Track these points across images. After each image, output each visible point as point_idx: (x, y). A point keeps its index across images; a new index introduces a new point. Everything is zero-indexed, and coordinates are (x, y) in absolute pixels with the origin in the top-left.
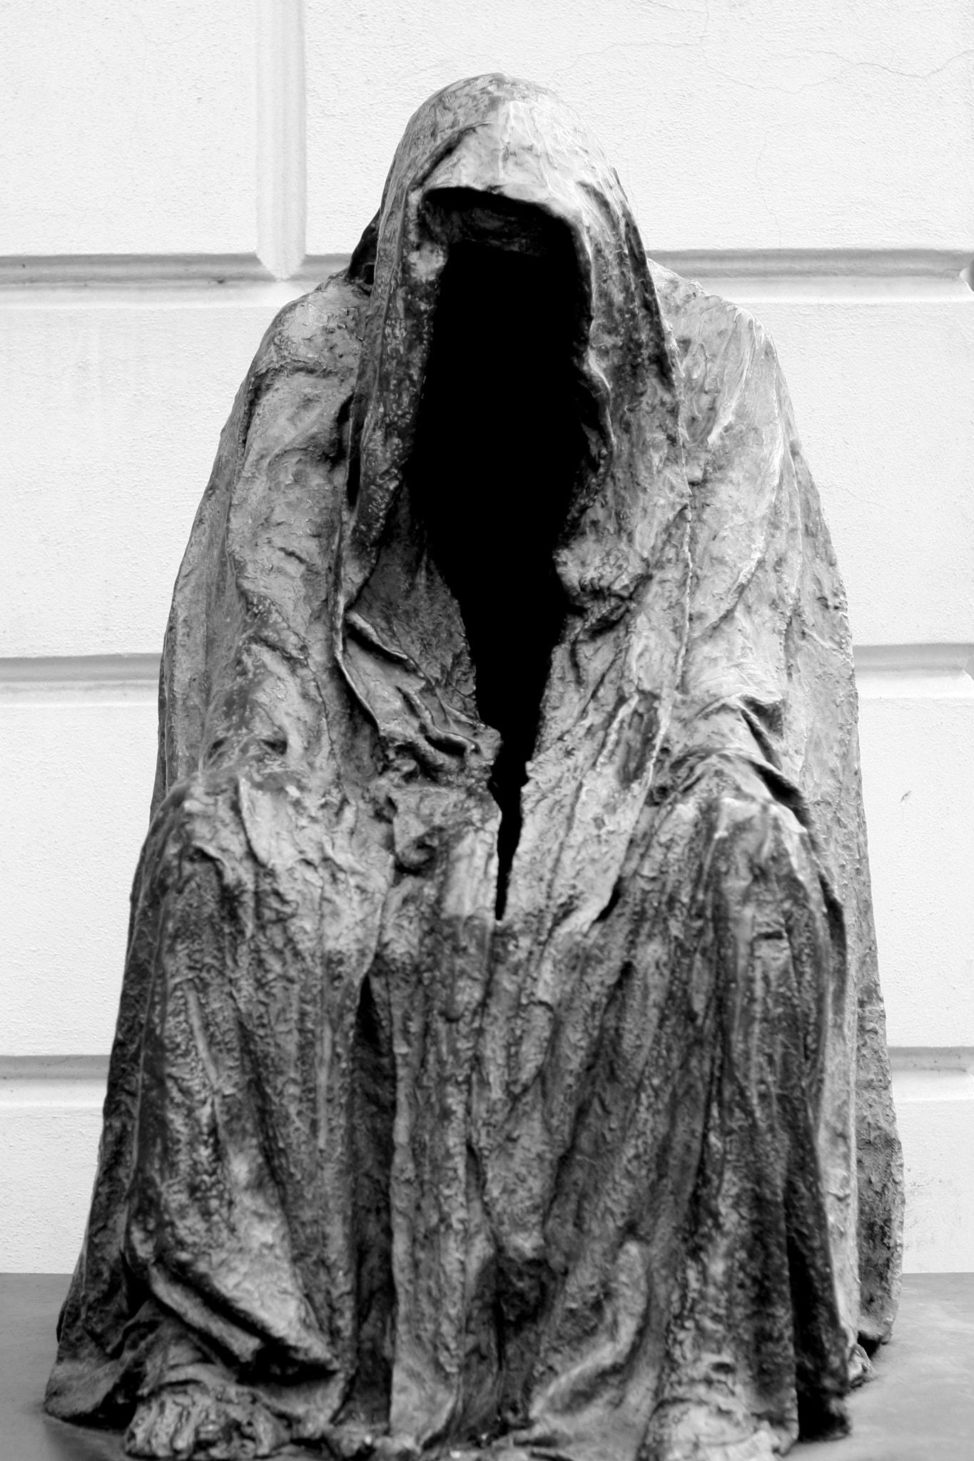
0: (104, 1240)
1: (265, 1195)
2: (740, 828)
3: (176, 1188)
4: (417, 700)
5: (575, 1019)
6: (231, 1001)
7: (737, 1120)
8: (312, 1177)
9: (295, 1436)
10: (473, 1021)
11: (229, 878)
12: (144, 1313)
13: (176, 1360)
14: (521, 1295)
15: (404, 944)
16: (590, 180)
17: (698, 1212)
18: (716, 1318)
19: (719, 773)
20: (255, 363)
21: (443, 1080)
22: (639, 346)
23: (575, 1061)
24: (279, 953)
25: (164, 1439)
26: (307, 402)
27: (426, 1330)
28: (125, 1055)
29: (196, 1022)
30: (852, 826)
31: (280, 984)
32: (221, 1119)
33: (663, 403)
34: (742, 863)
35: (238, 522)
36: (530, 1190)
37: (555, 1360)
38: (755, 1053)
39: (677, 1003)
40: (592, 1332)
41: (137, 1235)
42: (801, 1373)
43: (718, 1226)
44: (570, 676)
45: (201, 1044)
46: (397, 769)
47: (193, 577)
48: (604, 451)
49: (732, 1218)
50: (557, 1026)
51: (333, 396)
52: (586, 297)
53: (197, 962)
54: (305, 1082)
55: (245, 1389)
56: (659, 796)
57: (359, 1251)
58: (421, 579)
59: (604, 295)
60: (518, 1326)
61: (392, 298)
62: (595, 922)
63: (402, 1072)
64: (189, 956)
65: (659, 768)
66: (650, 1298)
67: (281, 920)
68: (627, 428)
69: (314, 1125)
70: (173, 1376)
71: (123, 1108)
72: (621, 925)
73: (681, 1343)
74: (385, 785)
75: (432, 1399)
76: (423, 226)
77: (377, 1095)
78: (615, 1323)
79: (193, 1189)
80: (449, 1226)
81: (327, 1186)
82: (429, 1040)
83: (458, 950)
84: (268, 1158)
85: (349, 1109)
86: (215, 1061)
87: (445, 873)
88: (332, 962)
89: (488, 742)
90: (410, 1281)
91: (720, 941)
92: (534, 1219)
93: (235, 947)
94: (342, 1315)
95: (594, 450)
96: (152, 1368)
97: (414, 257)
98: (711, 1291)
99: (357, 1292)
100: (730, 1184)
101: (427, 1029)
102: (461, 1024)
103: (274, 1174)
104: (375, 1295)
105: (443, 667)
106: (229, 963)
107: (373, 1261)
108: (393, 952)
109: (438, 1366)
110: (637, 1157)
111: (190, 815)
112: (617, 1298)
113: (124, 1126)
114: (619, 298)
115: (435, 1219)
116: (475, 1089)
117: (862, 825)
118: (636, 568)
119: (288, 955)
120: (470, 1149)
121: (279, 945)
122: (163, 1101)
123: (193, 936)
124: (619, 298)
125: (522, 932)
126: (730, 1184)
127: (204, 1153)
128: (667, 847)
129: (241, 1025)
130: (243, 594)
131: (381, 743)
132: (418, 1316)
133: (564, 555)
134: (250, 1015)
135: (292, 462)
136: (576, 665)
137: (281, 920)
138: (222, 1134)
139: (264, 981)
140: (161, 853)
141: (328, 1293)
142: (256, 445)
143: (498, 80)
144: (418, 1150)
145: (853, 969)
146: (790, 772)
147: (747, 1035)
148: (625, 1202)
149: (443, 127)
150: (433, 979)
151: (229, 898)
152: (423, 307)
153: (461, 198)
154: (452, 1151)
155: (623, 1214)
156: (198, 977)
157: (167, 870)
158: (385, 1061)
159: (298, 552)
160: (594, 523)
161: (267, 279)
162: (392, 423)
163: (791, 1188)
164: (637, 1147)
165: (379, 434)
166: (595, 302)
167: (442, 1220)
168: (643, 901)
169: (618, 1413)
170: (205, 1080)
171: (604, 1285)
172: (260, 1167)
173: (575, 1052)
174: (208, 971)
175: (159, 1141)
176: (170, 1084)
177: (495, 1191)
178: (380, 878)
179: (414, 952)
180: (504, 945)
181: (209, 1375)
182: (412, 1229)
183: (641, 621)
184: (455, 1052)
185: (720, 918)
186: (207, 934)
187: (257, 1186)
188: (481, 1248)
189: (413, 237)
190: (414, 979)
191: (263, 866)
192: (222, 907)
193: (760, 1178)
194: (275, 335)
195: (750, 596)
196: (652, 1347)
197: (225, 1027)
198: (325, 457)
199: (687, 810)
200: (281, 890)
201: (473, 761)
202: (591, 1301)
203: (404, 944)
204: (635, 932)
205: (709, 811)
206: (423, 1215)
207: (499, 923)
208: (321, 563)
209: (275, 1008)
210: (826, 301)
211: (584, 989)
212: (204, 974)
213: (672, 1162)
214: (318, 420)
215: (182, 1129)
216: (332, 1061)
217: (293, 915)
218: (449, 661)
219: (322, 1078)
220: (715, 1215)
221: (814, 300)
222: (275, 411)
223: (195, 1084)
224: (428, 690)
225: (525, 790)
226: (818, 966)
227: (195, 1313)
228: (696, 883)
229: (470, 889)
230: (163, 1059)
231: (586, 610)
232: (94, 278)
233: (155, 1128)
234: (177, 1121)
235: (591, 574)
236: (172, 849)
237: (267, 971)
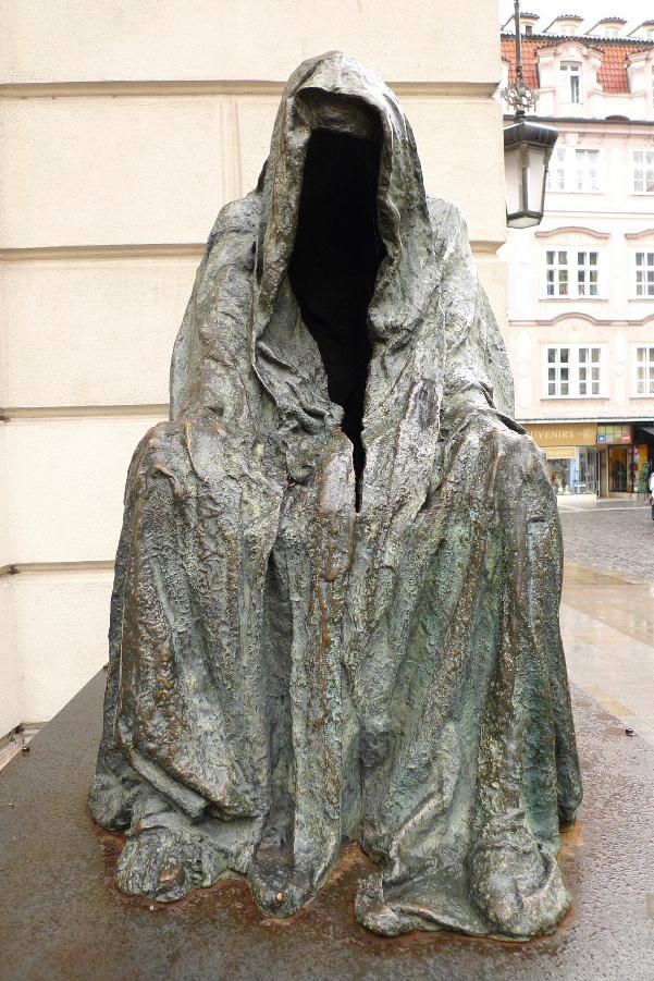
4: (297, 388)
10: (343, 580)
11: (179, 488)
15: (296, 528)
22: (412, 198)
29: (159, 584)
32: (177, 648)
33: (424, 231)
39: (475, 560)
43: (512, 717)
44: (381, 374)
45: (163, 598)
46: (287, 426)
49: (520, 709)
50: (397, 581)
51: (247, 241)
54: (232, 624)
58: (297, 330)
60: (373, 769)
62: (420, 511)
63: (296, 613)
69: (238, 651)
72: (441, 515)
76: (295, 116)
79: (157, 699)
80: (331, 719)
81: (249, 688)
84: (210, 671)
88: (249, 543)
89: (338, 411)
95: (390, 253)
98: (510, 763)
103: (214, 680)
104: (282, 754)
105: (310, 375)
106: (181, 545)
107: (280, 729)
110: (454, 669)
114: (403, 168)
115: (321, 714)
116: (345, 625)
118: (414, 315)
119: (220, 541)
120: (343, 666)
121: (213, 533)
123: (156, 528)
124: (403, 168)
127: (165, 674)
128: (465, 463)
129: (190, 587)
131: (279, 411)
136: (384, 368)
137: (214, 516)
138: (179, 658)
141: (251, 758)
151: (179, 502)
158: (285, 604)
160: (390, 295)
164: (455, 663)
167: (326, 716)
168: (452, 498)
170: (171, 621)
172: (205, 678)
174: (167, 551)
175: (134, 666)
180: (362, 529)
181: (170, 821)
185: (503, 509)
188: (352, 728)
197: (178, 587)
198: (245, 269)
200: (213, 495)
201: (330, 422)
207: (358, 515)
213: (473, 667)
218: (313, 372)
219: (243, 619)
220: (510, 709)
223: (158, 626)
224: (304, 383)
234: (146, 652)
237: (205, 550)
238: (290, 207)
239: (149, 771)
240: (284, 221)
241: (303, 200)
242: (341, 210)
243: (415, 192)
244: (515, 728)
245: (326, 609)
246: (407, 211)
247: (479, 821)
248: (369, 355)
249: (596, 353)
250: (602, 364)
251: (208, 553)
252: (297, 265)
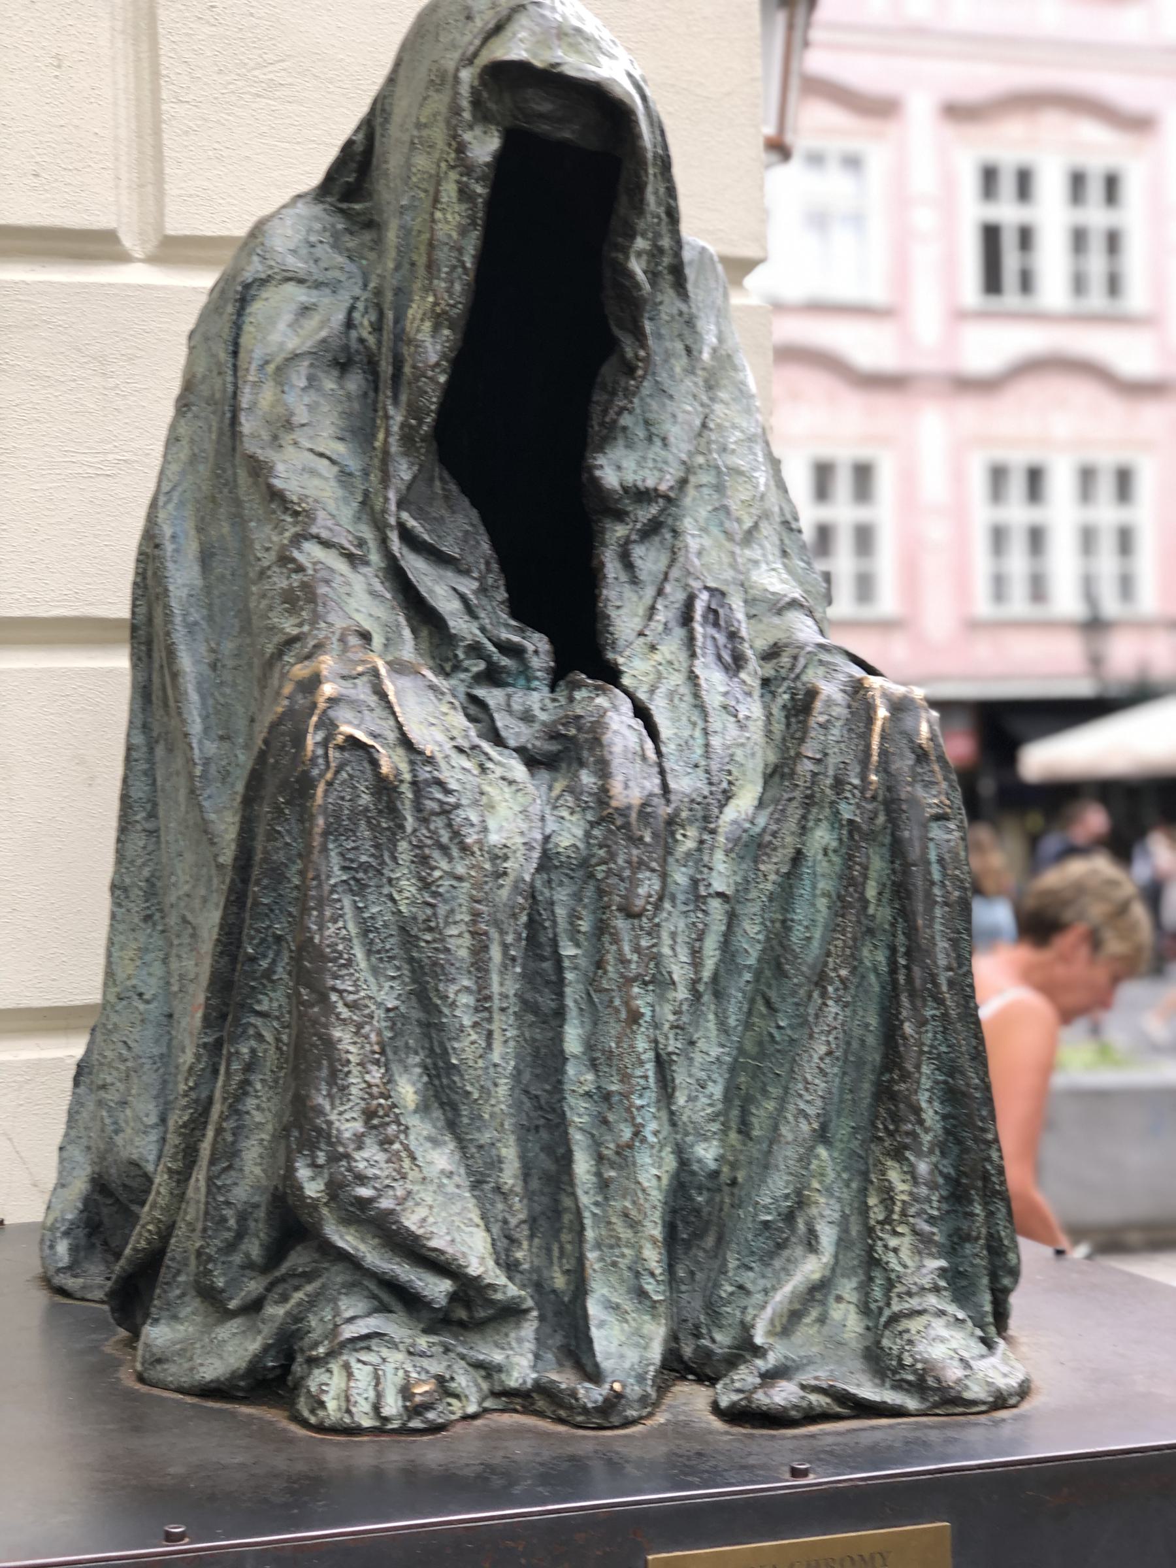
0: (228, 1182)
1: (431, 1119)
3: (347, 1116)
5: (753, 910)
6: (390, 904)
9: (498, 1388)
13: (355, 1316)
23: (751, 954)
24: (444, 849)
25: (366, 1407)
27: (623, 1256)
28: (254, 972)
29: (353, 929)
31: (447, 883)
33: (681, 314)
36: (711, 1096)
39: (850, 882)
41: (303, 1172)
43: (921, 1122)
44: (624, 577)
45: (359, 953)
46: (467, 670)
47: (176, 496)
48: (642, 353)
53: (352, 861)
54: (479, 991)
55: (434, 1339)
64: (342, 854)
67: (446, 811)
70: (349, 1332)
71: (251, 1031)
73: (895, 1250)
75: (637, 1332)
76: (476, 103)
77: (536, 1002)
78: (812, 1233)
80: (644, 1140)
82: (606, 938)
86: (375, 971)
88: (498, 856)
90: (596, 1204)
92: (715, 1127)
93: (394, 843)
94: (520, 1244)
95: (629, 353)
102: (644, 920)
103: (446, 1097)
108: (557, 845)
110: (829, 1053)
112: (809, 1205)
113: (253, 1051)
115: (627, 1133)
119: (455, 852)
122: (327, 1017)
125: (691, 821)
132: (613, 1241)
133: (601, 460)
134: (415, 918)
135: (304, 366)
137: (446, 811)
139: (430, 880)
141: (505, 1222)
144: (595, 1058)
148: (819, 1103)
150: (609, 872)
151: (384, 788)
152: (479, 190)
154: (643, 1057)
155: (818, 1115)
156: (354, 878)
158: (546, 965)
159: (328, 453)
162: (445, 312)
165: (427, 325)
167: (636, 1134)
169: (826, 1330)
171: (799, 1193)
173: (752, 946)
176: (334, 997)
177: (681, 1099)
179: (581, 845)
181: (394, 1326)
182: (596, 1145)
186: (364, 831)
187: (423, 1108)
189: (467, 115)
190: (580, 874)
191: (421, 753)
192: (379, 800)
202: (785, 1211)
206: (610, 1130)
209: (442, 910)
211: (761, 879)
212: (360, 875)
214: (330, 315)
215: (352, 1049)
216: (505, 966)
217: (457, 806)
220: (917, 1110)
222: (272, 320)
227: (373, 1257)
230: (322, 970)
231: (627, 513)
234: (342, 1036)
238: (464, 267)
240: (449, 291)
241: (485, 258)
243: (666, 242)
244: (927, 1138)
245: (629, 961)
247: (877, 1293)
249: (863, 474)
250: (884, 512)
251: (437, 874)
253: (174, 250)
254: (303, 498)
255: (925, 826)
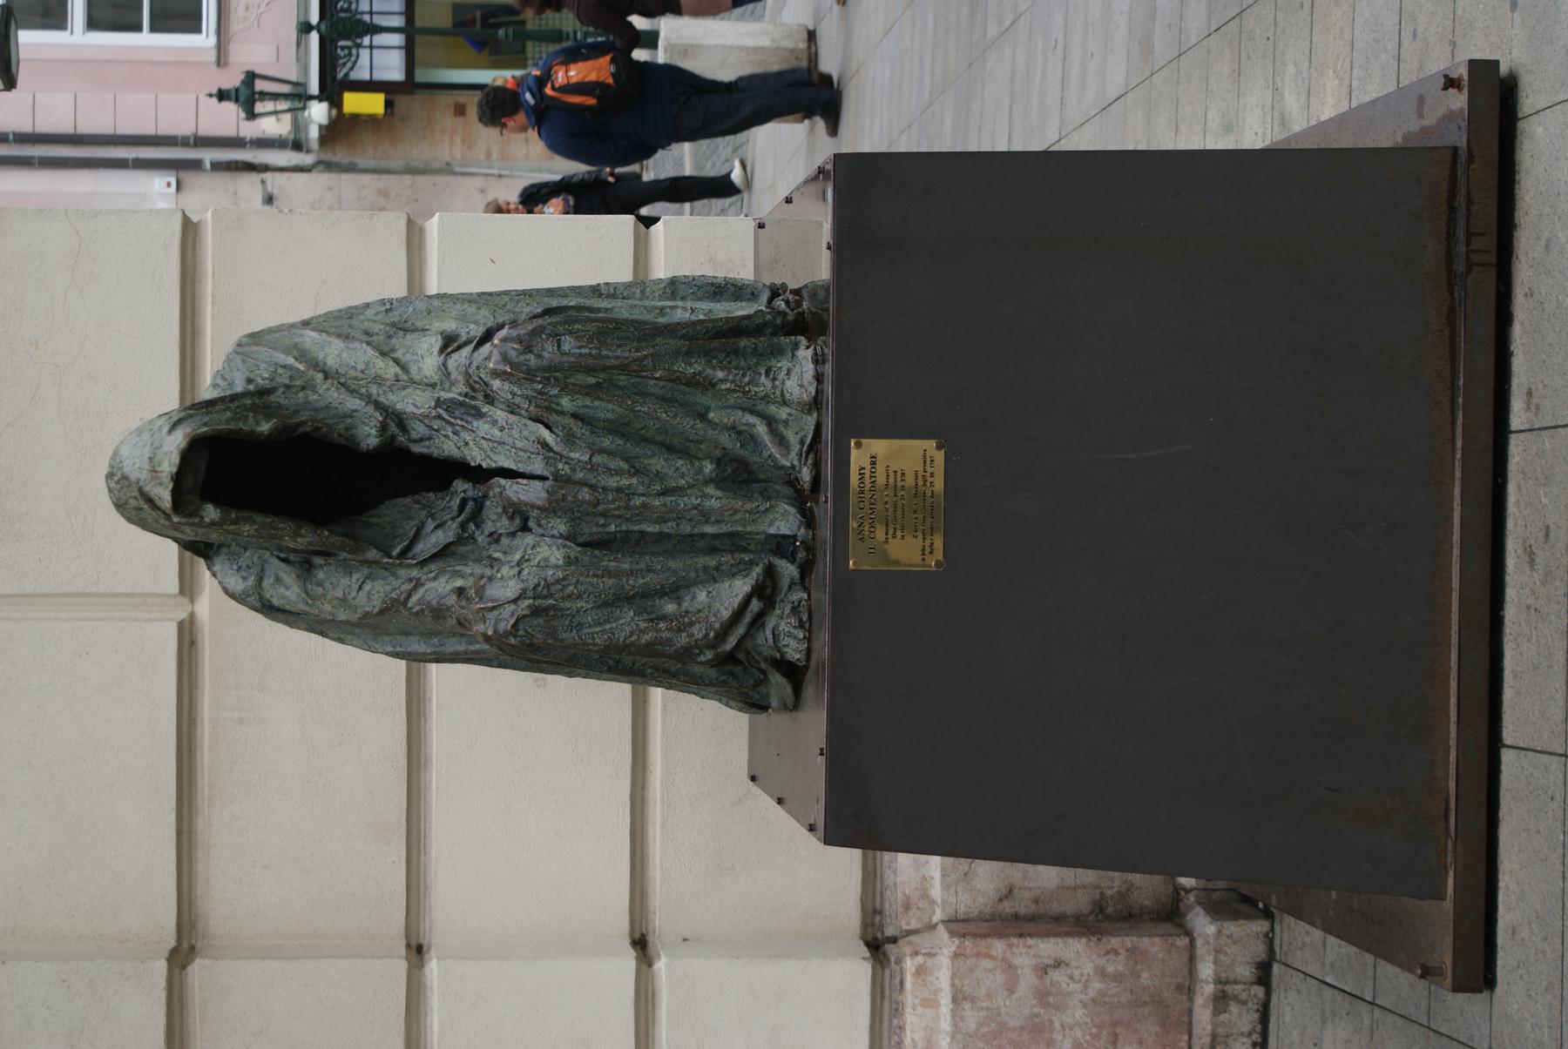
2: (505, 358)
7: (648, 362)
8: (675, 572)
11: (526, 612)
12: (741, 656)
13: (764, 638)
14: (734, 471)
15: (560, 526)
16: (166, 429)
17: (693, 382)
18: (744, 376)
19: (478, 368)
20: (257, 610)
21: (627, 507)
26: (278, 580)
29: (598, 629)
30: (506, 299)
34: (522, 358)
35: (343, 617)
37: (765, 454)
38: (615, 353)
39: (592, 391)
40: (752, 436)
41: (702, 658)
42: (774, 334)
45: (607, 627)
51: (275, 566)
52: (231, 431)
56: (490, 399)
57: (713, 550)
58: (375, 520)
59: (227, 422)
60: (751, 473)
61: (228, 532)
65: (469, 404)
66: (735, 407)
67: (548, 586)
68: (297, 412)
70: (771, 641)
72: (553, 418)
74: (481, 539)
76: (191, 515)
78: (748, 424)
79: (679, 630)
83: (564, 498)
85: (641, 554)
87: (526, 504)
88: (569, 561)
89: (461, 486)
91: (560, 370)
96: (767, 652)
97: (207, 520)
99: (732, 552)
100: (680, 366)
101: (603, 515)
103: (673, 591)
104: (735, 542)
107: (717, 544)
109: (767, 511)
111: (495, 631)
114: (229, 414)
117: (506, 293)
118: (370, 409)
124: (229, 414)
126: (680, 366)
127: (662, 625)
130: (382, 612)
131: (459, 540)
136: (421, 440)
137: (548, 586)
140: (513, 646)
142: (301, 607)
143: (110, 476)
144: (662, 520)
145: (582, 301)
146: (477, 331)
147: (607, 357)
149: (134, 504)
151: (536, 612)
153: (176, 494)
157: (523, 643)
161: (192, 616)
163: (683, 337)
166: (232, 426)
170: (626, 624)
178: (529, 539)
182: (700, 523)
183: (399, 407)
184: (614, 501)
185: (550, 369)
186: (554, 623)
188: (710, 490)
193: (677, 353)
194: (240, 598)
195: (386, 349)
196: (761, 406)
199: (496, 384)
201: (470, 494)
203: (560, 526)
204: (556, 412)
205: (496, 374)
208: (366, 571)
210: (210, 299)
214: (288, 575)
219: (626, 566)
220: (694, 374)
221: (209, 307)
224: (432, 516)
225: (484, 465)
226: (577, 321)
227: (740, 630)
228: (532, 381)
229: (531, 493)
232: (190, 715)
233: (650, 650)
234: (646, 638)
235: (373, 432)
236: (513, 641)
239: (732, 641)
242: (282, 482)
246: (267, 411)
248: (404, 453)
252: (318, 518)
253: (187, 587)
254: (384, 602)
255: (563, 354)
